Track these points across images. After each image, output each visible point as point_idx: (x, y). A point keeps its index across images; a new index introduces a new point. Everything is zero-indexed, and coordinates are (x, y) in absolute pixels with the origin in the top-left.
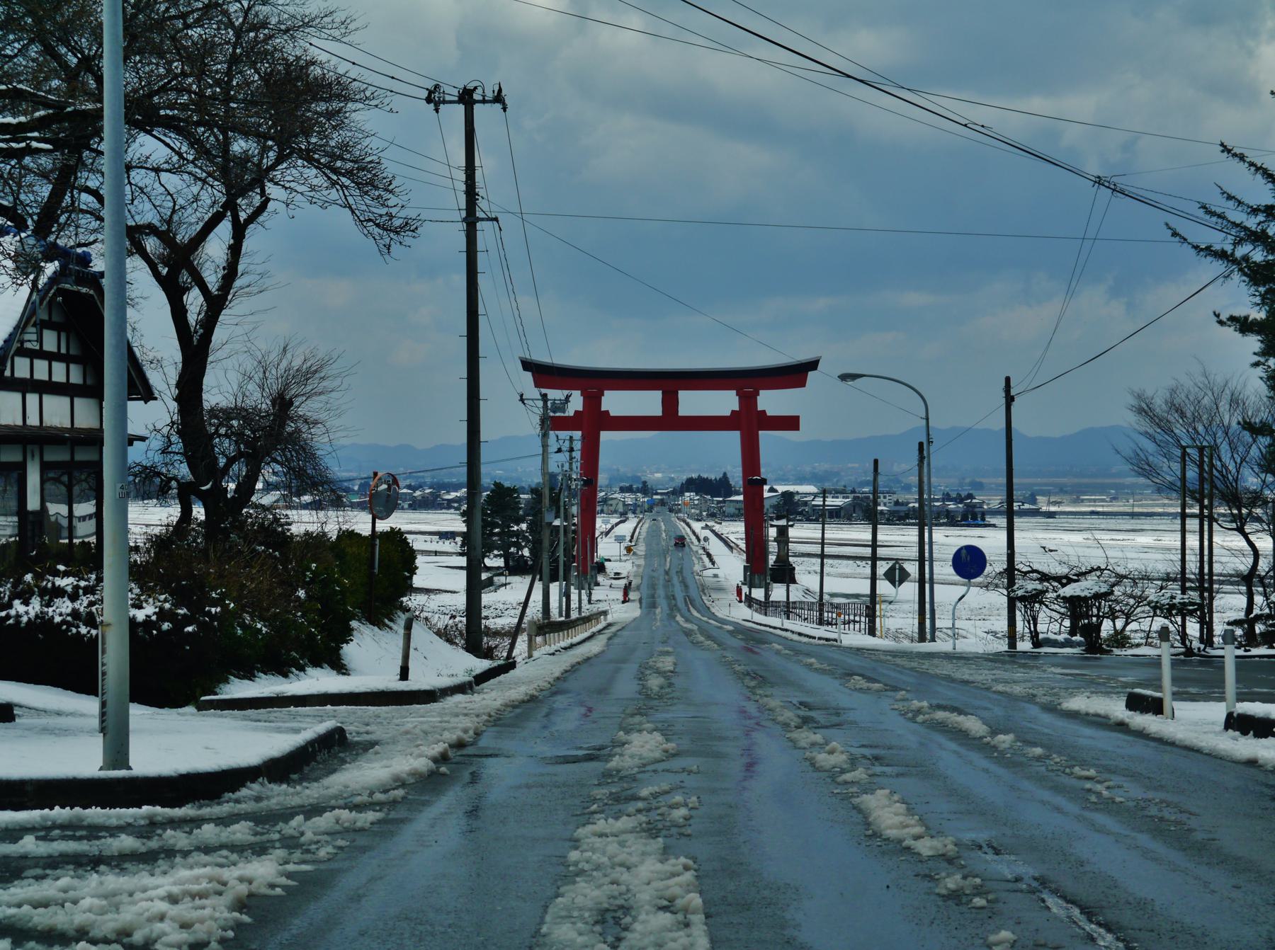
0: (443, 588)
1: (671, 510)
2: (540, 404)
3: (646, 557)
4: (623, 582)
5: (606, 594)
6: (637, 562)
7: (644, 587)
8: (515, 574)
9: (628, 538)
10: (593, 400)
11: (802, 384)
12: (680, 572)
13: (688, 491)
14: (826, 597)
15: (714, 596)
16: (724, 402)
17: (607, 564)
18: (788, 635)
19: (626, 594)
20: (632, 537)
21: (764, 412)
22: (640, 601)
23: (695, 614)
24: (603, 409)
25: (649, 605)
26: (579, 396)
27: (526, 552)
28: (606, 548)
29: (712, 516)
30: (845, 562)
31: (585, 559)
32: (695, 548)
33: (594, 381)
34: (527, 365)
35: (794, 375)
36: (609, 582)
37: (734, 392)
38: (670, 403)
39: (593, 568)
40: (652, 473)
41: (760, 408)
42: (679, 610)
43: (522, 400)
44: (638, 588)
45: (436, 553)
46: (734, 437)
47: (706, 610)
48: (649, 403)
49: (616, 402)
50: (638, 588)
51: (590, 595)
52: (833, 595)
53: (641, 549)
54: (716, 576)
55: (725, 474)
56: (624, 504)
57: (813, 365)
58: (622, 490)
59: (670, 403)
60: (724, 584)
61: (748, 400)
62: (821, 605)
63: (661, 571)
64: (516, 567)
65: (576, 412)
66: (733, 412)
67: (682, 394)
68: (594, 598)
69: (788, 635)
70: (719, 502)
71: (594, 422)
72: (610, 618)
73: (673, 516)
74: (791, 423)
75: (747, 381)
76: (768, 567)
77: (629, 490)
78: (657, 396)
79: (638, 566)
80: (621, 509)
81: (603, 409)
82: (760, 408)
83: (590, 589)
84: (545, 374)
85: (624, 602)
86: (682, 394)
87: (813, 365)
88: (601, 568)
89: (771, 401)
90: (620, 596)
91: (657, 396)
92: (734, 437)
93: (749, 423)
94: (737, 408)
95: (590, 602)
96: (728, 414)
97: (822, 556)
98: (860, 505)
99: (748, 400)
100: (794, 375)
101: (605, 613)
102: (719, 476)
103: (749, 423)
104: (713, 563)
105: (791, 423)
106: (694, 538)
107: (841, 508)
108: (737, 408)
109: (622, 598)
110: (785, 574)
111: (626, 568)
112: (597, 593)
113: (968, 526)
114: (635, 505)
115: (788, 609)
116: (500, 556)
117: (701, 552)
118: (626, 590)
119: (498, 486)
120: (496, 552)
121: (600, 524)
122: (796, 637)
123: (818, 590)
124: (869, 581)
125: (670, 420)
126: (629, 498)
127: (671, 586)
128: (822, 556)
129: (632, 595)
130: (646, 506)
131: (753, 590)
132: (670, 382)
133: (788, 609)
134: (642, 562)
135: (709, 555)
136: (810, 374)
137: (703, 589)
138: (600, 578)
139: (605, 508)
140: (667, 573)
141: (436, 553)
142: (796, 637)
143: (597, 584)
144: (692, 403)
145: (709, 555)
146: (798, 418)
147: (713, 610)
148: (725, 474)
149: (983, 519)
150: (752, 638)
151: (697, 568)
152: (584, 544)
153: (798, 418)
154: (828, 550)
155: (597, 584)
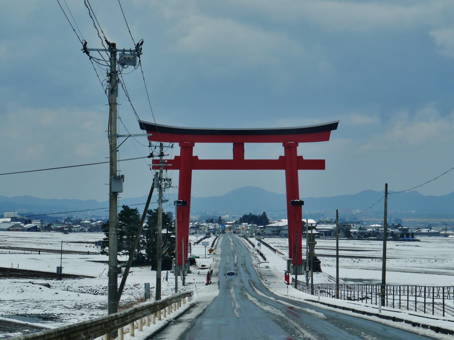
0: (86, 274)
1: (234, 233)
2: (107, 56)
3: (222, 256)
4: (206, 271)
5: (195, 278)
6: (216, 259)
7: (221, 274)
8: (136, 266)
9: (211, 245)
10: (187, 149)
11: (327, 138)
12: (244, 265)
13: (244, 222)
14: (341, 282)
15: (269, 280)
16: (275, 150)
17: (197, 260)
18: (421, 331)
19: (209, 278)
20: (213, 244)
21: (301, 157)
22: (219, 283)
23: (259, 293)
24: (194, 155)
25: (225, 289)
26: (180, 148)
27: (143, 252)
28: (196, 251)
29: (259, 234)
30: (346, 259)
31: (180, 255)
32: (252, 251)
33: (187, 137)
34: (143, 126)
35: (321, 133)
36: (198, 271)
37: (281, 144)
38: (239, 150)
39: (186, 261)
40: (224, 215)
41: (299, 154)
42: (247, 290)
43: (86, 50)
44: (217, 275)
45: (88, 253)
46: (281, 174)
47: (266, 290)
48: (225, 151)
49: (202, 150)
50: (217, 275)
51: (184, 279)
52: (345, 280)
53: (218, 251)
54: (267, 267)
55: (264, 213)
56: (209, 229)
57: (334, 126)
58: (207, 222)
59: (239, 150)
60: (274, 272)
61: (290, 149)
62: (338, 285)
63: (232, 265)
64: (138, 262)
65: (176, 157)
66: (280, 157)
67: (247, 146)
68: (187, 281)
69: (421, 331)
70: (261, 228)
71: (187, 164)
72: (195, 298)
73: (236, 236)
74: (319, 165)
75: (290, 137)
76: (303, 263)
77: (211, 221)
78: (230, 146)
79: (217, 261)
80: (207, 231)
81: (194, 155)
82: (299, 154)
83: (184, 275)
84: (156, 132)
85: (207, 284)
86: (247, 146)
87: (334, 126)
88: (192, 262)
89: (306, 150)
90: (205, 280)
91: (230, 146)
92: (281, 174)
93: (291, 165)
94: (283, 155)
95: (184, 284)
96: (277, 158)
97: (338, 256)
98: (343, 229)
99: (290, 149)
100: (321, 133)
101: (189, 294)
102: (261, 214)
103: (291, 165)
104: (265, 259)
105: (319, 165)
106: (251, 246)
107: (331, 230)
108: (283, 155)
109: (205, 281)
110: (315, 266)
111: (209, 262)
112: (188, 279)
113: (404, 240)
114: (215, 229)
115: (323, 289)
116: (126, 254)
117: (256, 252)
118: (209, 276)
119: (125, 207)
120: (124, 251)
121: (192, 238)
122: (429, 332)
123: (335, 276)
124: (381, 272)
125: (239, 162)
126: (211, 226)
127: (237, 276)
128: (338, 256)
129: (213, 280)
130: (221, 230)
131: (298, 276)
132: (238, 137)
133: (323, 289)
134: (219, 258)
135: (261, 255)
136: (332, 132)
137: (261, 276)
138: (192, 268)
139: (198, 231)
140: (236, 265)
141: (88, 253)
142: (429, 332)
143: (190, 272)
144: (253, 151)
145: (261, 255)
146: (324, 160)
147: (272, 290)
148: (264, 213)
149: (413, 237)
150: (294, 310)
151: (255, 262)
152: (180, 244)
153: (324, 160)
154: (340, 253)
155: (190, 272)
